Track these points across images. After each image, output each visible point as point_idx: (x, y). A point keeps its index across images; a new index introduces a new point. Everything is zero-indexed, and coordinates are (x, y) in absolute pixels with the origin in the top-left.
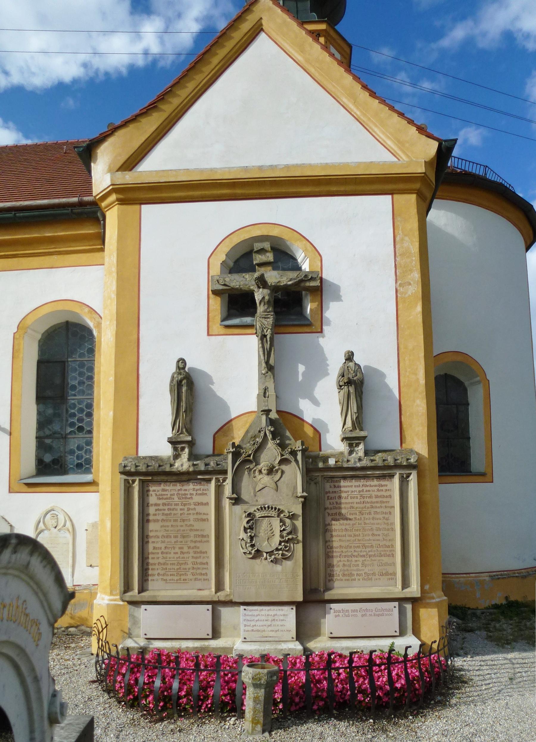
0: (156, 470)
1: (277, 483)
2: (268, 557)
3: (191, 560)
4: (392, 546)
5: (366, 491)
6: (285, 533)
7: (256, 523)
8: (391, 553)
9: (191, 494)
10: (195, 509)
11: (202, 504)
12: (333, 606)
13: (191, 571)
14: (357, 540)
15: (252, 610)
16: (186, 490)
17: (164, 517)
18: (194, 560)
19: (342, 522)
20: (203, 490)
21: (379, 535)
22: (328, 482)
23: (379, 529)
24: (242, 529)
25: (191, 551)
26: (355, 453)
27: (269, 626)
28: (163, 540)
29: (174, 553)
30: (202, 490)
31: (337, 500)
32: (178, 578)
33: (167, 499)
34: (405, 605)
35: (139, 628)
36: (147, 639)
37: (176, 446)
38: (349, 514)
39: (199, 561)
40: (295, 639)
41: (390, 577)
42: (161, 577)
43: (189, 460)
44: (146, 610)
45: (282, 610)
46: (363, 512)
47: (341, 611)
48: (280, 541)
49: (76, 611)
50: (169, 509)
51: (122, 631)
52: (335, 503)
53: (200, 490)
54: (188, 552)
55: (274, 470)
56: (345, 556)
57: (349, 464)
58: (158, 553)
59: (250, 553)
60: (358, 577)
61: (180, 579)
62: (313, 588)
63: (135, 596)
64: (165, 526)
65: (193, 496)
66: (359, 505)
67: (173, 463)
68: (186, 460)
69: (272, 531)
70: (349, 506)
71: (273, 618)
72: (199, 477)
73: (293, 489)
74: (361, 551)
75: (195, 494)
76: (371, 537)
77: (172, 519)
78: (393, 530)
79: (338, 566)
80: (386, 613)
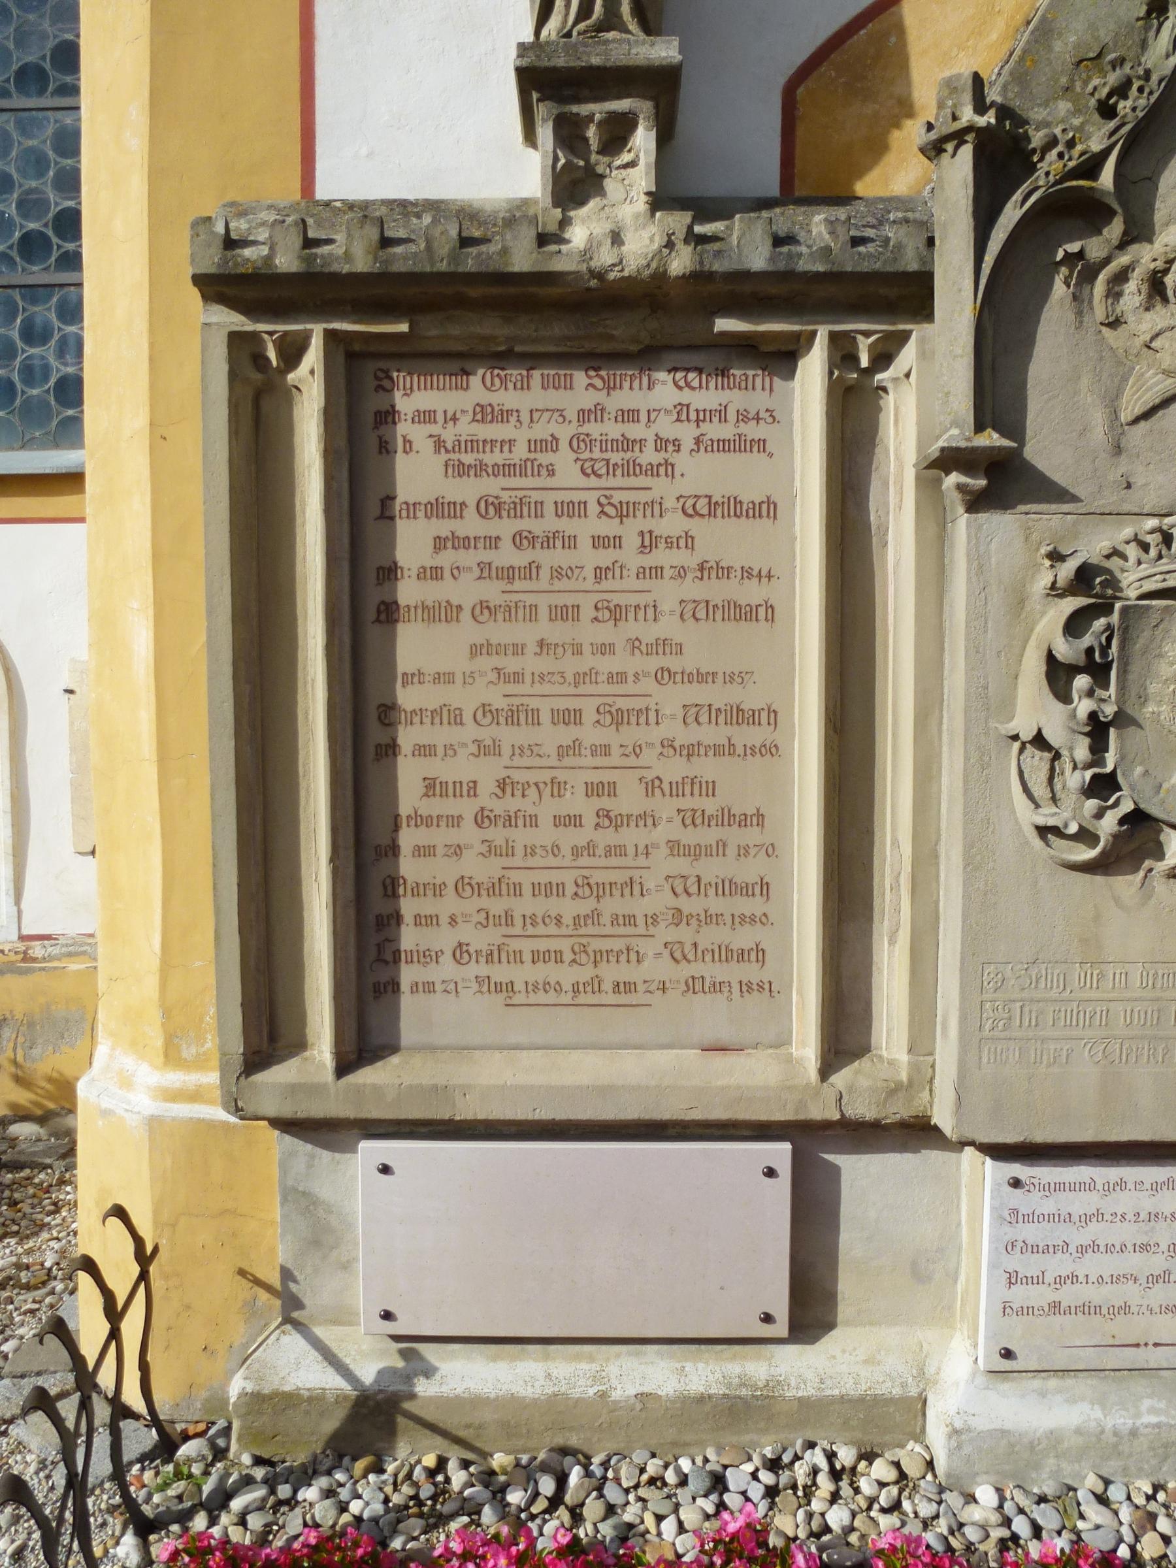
0: (443, 267)
3: (664, 865)
7: (1125, 630)
9: (662, 443)
10: (689, 540)
11: (734, 508)
13: (665, 932)
15: (1060, 1187)
16: (629, 416)
17: (492, 591)
18: (681, 865)
20: (743, 417)
24: (1033, 667)
25: (666, 807)
27: (1154, 1279)
28: (486, 734)
29: (558, 821)
30: (731, 416)
32: (585, 973)
33: (507, 469)
35: (346, 1266)
36: (397, 1338)
37: (575, 109)
39: (712, 869)
42: (476, 969)
43: (659, 201)
44: (385, 1170)
49: (36, 1052)
50: (519, 539)
51: (242, 1273)
53: (724, 419)
54: (643, 816)
58: (455, 821)
59: (1086, 836)
61: (595, 985)
63: (314, 1090)
64: (500, 650)
65: (675, 459)
67: (552, 227)
68: (641, 204)
72: (725, 324)
75: (688, 443)
77: (543, 602)
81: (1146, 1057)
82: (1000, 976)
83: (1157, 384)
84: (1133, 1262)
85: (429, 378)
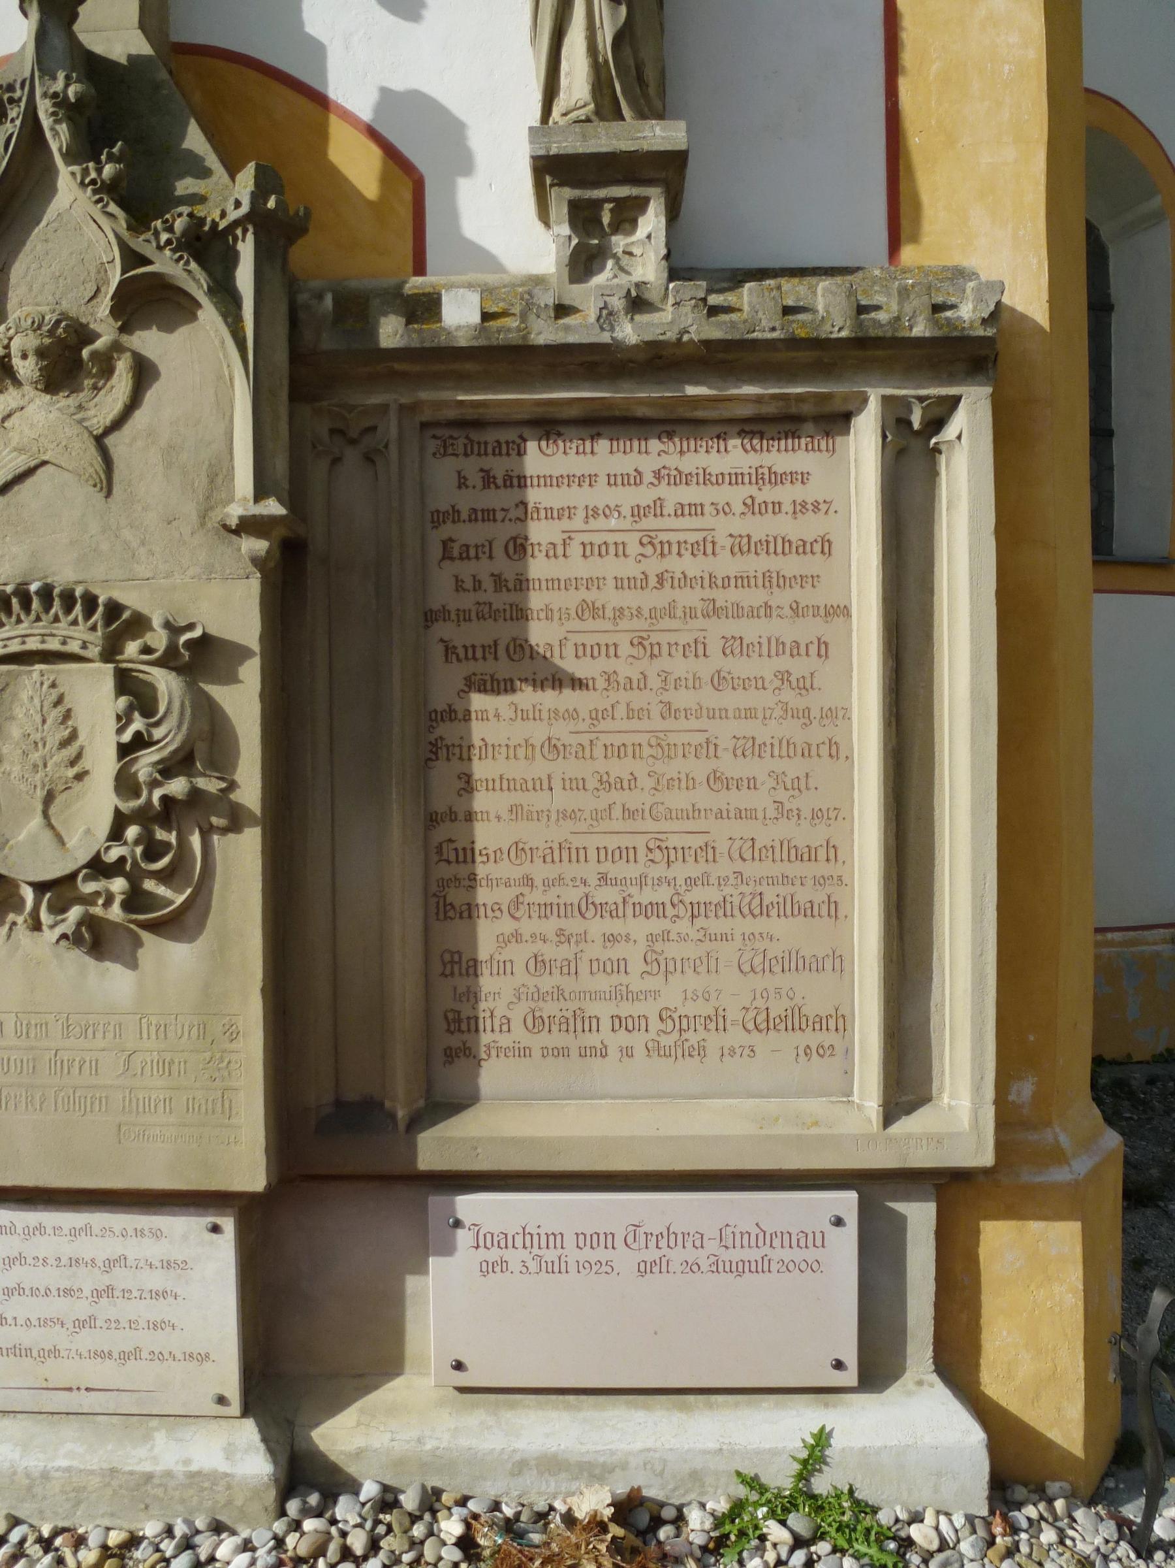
1: (109, 441)
2: (45, 917)
4: (833, 851)
5: (681, 510)
6: (145, 764)
8: (819, 897)
12: (469, 1205)
14: (617, 812)
19: (526, 696)
21: (752, 784)
22: (445, 450)
23: (751, 748)
26: (610, 263)
27: (80, 1324)
31: (501, 564)
34: (900, 1207)
38: (569, 651)
40: (235, 1408)
41: (813, 1038)
45: (157, 1234)
46: (655, 638)
47: (519, 1241)
48: (118, 812)
52: (488, 584)
55: (85, 353)
56: (547, 910)
57: (567, 328)
60: (623, 1038)
62: (351, 1096)
66: (630, 599)
69: (71, 751)
70: (570, 599)
71: (106, 1280)
73: (205, 480)
74: (642, 882)
76: (703, 797)
78: (837, 751)
79: (505, 968)
80: (787, 1254)
81: (24, 1105)
82: (234, 1027)
83: (10, 461)
84: (57, 1306)
85: (628, 443)
